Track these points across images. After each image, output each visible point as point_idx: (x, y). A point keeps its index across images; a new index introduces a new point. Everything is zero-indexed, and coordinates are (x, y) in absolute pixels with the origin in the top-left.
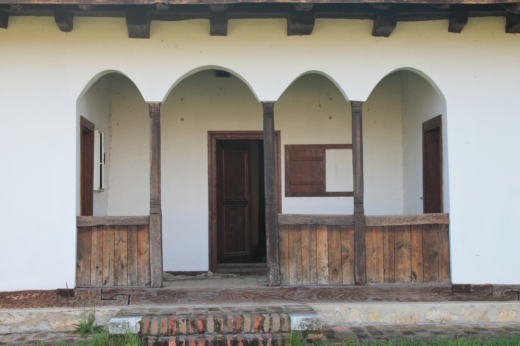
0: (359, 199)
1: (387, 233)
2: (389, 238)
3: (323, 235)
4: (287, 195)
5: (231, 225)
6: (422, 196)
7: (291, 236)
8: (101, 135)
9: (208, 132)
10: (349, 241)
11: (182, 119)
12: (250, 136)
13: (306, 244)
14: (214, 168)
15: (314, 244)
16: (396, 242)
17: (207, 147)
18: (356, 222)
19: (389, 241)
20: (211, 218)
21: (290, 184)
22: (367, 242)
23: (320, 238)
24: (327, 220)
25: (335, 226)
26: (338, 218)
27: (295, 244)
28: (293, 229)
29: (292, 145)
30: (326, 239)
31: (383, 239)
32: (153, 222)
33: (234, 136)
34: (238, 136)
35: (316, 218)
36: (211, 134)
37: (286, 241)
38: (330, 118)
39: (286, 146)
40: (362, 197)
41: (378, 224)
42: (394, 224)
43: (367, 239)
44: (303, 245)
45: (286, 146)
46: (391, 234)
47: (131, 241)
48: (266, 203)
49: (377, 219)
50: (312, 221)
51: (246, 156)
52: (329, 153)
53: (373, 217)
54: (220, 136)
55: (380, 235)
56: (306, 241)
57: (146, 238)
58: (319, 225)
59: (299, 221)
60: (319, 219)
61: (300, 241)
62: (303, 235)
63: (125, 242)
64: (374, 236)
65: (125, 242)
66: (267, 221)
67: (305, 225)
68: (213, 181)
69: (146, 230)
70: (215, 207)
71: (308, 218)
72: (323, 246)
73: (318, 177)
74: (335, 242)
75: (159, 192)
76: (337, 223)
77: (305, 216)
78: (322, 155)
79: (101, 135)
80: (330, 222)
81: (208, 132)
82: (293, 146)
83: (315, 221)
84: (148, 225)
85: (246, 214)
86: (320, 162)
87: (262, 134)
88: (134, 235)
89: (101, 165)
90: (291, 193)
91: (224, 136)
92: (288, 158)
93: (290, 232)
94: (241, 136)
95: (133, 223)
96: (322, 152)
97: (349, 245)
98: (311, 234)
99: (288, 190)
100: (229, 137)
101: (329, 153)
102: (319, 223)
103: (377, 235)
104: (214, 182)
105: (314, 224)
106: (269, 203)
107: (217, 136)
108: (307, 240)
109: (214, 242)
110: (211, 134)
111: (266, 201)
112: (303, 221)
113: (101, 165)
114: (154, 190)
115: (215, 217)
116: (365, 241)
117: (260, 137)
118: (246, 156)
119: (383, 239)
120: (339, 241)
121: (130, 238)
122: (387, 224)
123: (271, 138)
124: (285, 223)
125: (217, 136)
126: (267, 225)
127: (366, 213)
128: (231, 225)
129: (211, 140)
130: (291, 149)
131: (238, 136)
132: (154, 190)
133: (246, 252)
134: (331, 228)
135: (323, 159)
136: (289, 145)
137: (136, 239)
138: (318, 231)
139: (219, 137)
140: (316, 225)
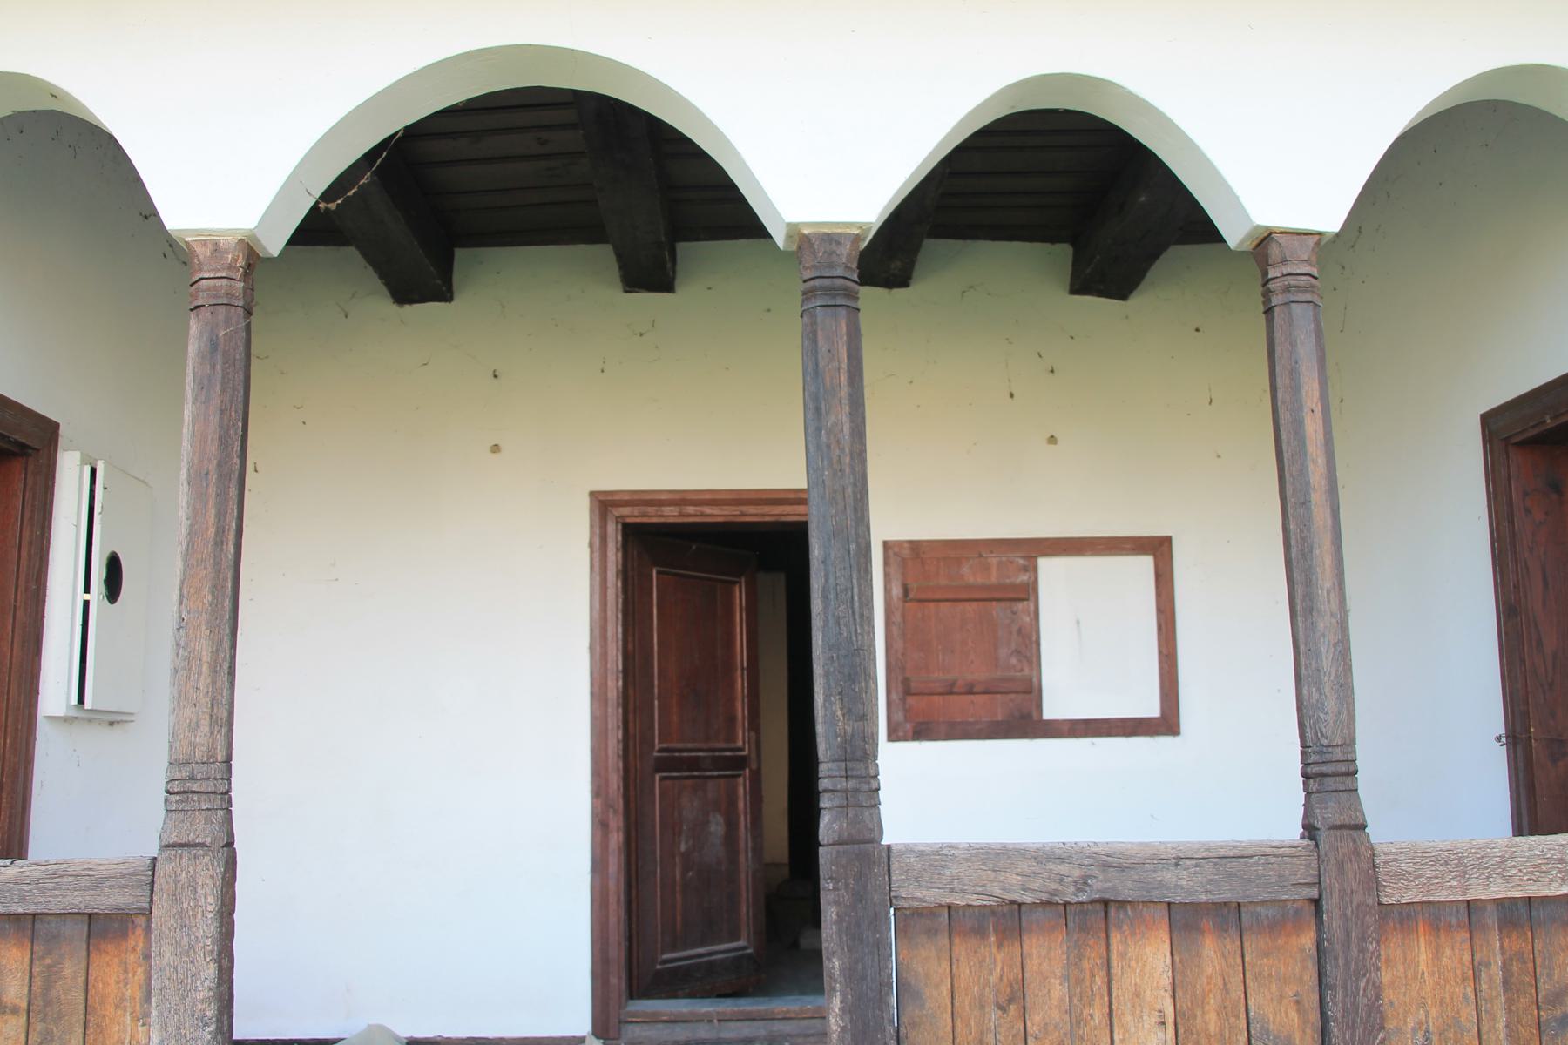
0: (1338, 754)
1: (1495, 935)
2: (1505, 967)
3: (1148, 960)
4: (893, 736)
5: (683, 847)
6: (1503, 732)
7: (965, 972)
8: (93, 471)
9: (592, 494)
10: (1290, 992)
11: (496, 449)
12: (751, 510)
13: (1056, 1015)
14: (615, 630)
15: (1098, 1013)
16: (1545, 988)
17: (587, 551)
18: (1326, 881)
19: (1506, 983)
20: (600, 824)
21: (907, 692)
22: (1388, 994)
23: (1125, 982)
24: (1169, 876)
25: (1207, 907)
26: (1227, 860)
27: (993, 1015)
28: (980, 932)
29: (911, 542)
30: (1166, 980)
31: (1476, 977)
32: (175, 898)
33: (691, 509)
34: (707, 510)
35: (1106, 866)
36: (604, 504)
37: (937, 996)
38: (1052, 440)
39: (886, 544)
40: (1350, 743)
41: (1449, 892)
42: (1533, 891)
43: (1386, 976)
44: (1035, 1021)
45: (886, 544)
46: (1516, 943)
47: (48, 1003)
48: (824, 784)
49: (1436, 861)
50: (1084, 880)
51: (739, 595)
52: (1050, 569)
53: (1421, 856)
54: (636, 510)
55: (1456, 953)
56: (1051, 996)
57: (133, 991)
58: (1122, 904)
59: (1011, 886)
60: (1121, 868)
61: (1016, 997)
62: (1033, 965)
63: (15, 1011)
64: (1423, 957)
65: (15, 1011)
66: (826, 885)
67: (1045, 904)
68: (611, 684)
69: (136, 940)
70: (615, 781)
71: (1063, 869)
72: (1150, 1020)
73: (1014, 661)
74: (1213, 1002)
75: (226, 722)
76: (1228, 893)
77: (1043, 856)
78: (1024, 578)
79: (93, 471)
80: (1186, 886)
81: (592, 494)
82: (915, 546)
83: (1100, 886)
84: (148, 913)
85: (741, 805)
86: (1020, 606)
87: (803, 502)
88: (71, 969)
89: (86, 604)
90: (908, 726)
91: (651, 510)
92: (897, 591)
93: (960, 949)
94: (715, 511)
95: (57, 904)
96: (1025, 569)
97: (1293, 1014)
98: (1081, 957)
99: (899, 716)
100: (670, 514)
101: (1050, 569)
102: (1127, 892)
103: (1437, 953)
104: (614, 686)
105: (1091, 904)
106: (842, 784)
107: (625, 511)
108: (1058, 990)
109: (613, 920)
110: (604, 504)
111: (823, 769)
112: (1036, 884)
113: (86, 604)
114: (189, 712)
115: (616, 822)
116: (1378, 988)
117: (789, 513)
118: (739, 595)
119: (1476, 977)
120: (1237, 993)
121: (48, 985)
122: (1497, 891)
123: (845, 419)
124: (932, 895)
125: (625, 511)
126: (829, 913)
127: (1382, 832)
128: (683, 847)
129: (604, 527)
130: (912, 558)
131: (707, 510)
132: (189, 712)
133: (742, 943)
134: (1186, 920)
135: (1027, 593)
136: (900, 543)
137: (80, 996)
138: (1116, 938)
139: (633, 514)
140: (1106, 903)
